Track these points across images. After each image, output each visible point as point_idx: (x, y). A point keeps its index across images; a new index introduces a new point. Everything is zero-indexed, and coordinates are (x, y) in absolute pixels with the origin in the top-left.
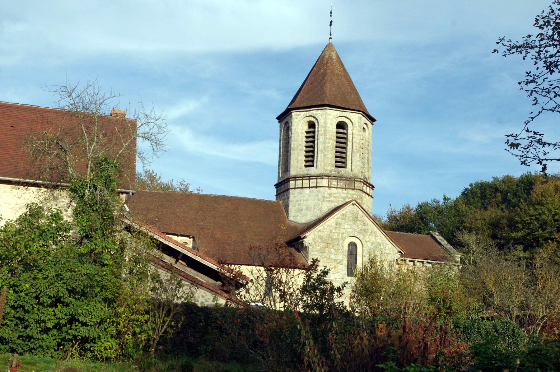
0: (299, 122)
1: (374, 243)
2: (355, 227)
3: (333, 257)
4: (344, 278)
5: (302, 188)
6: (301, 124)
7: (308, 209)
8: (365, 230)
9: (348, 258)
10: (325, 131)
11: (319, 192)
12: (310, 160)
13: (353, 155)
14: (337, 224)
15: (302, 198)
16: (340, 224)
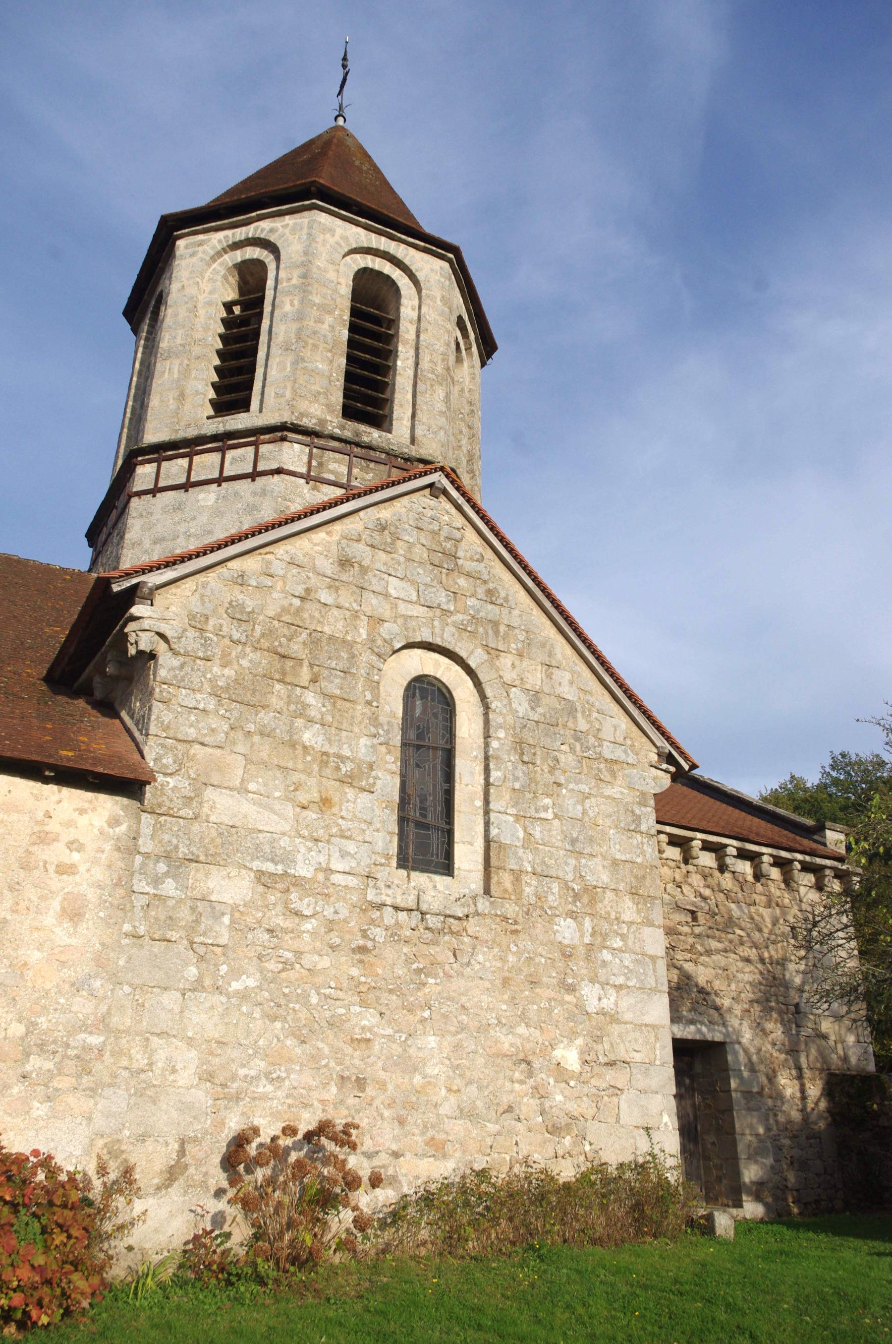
0: (202, 279)
1: (545, 700)
2: (442, 598)
3: (310, 736)
4: (382, 874)
6: (208, 275)
8: (495, 624)
9: (405, 762)
10: (305, 276)
12: (235, 382)
13: (421, 387)
14: (345, 563)
15: (182, 528)
16: (364, 570)
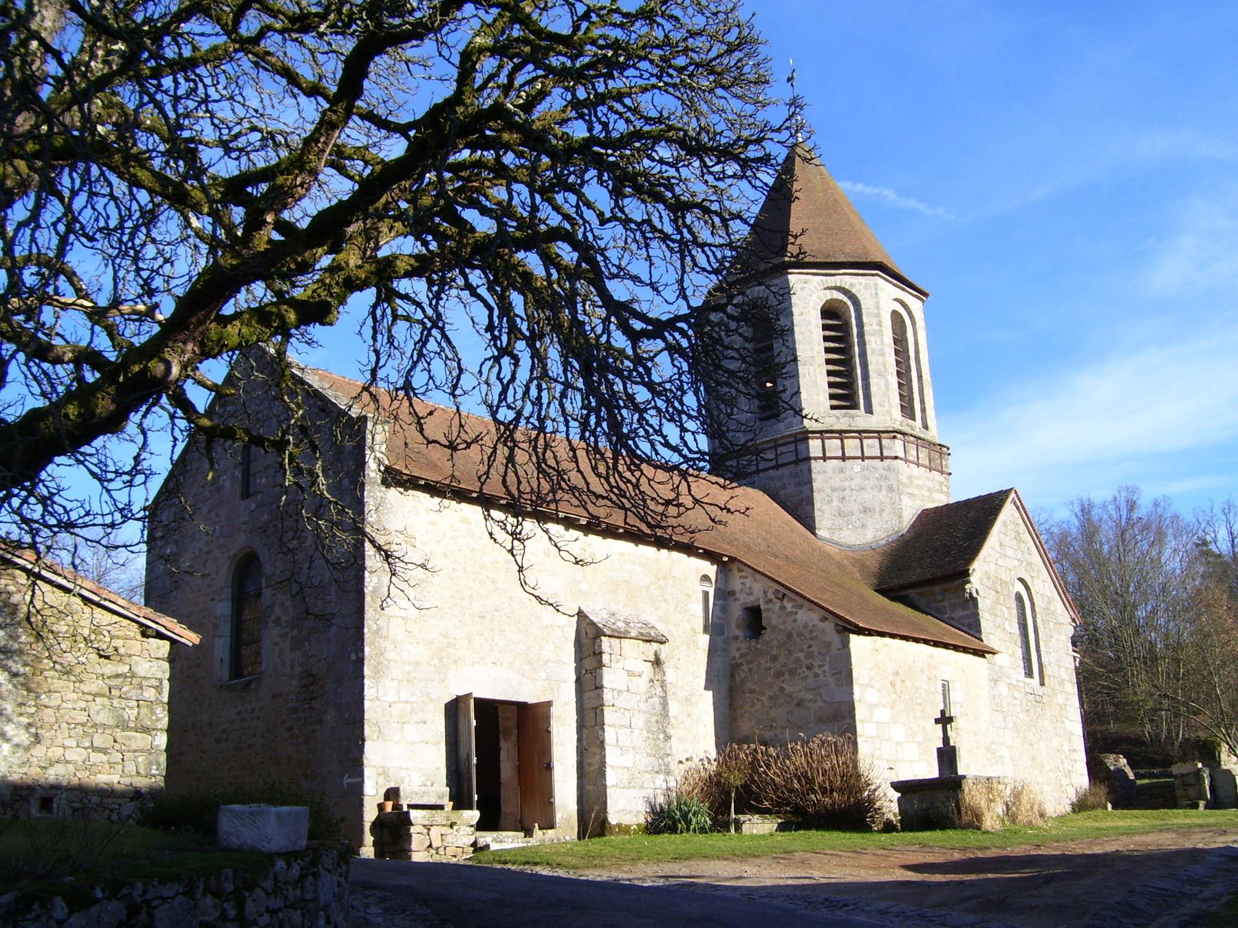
5: (843, 458)
7: (865, 511)
11: (889, 469)
12: (847, 390)
